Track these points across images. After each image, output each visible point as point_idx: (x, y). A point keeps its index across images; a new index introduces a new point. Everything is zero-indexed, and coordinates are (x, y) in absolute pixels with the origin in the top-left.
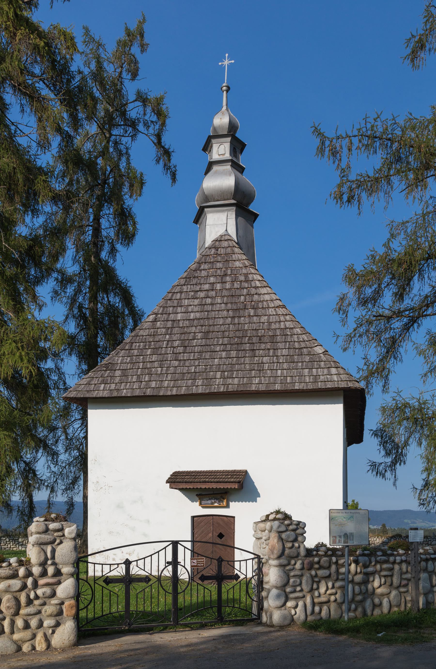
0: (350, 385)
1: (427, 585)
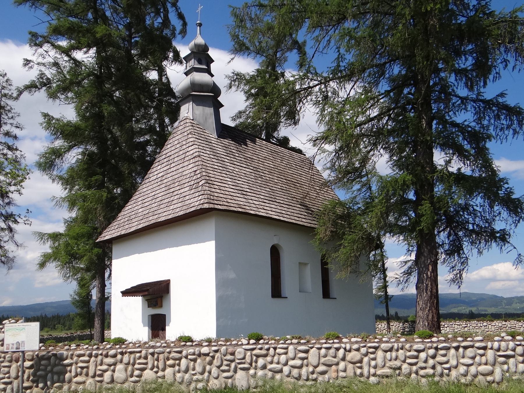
0: (188, 211)
1: (121, 375)
